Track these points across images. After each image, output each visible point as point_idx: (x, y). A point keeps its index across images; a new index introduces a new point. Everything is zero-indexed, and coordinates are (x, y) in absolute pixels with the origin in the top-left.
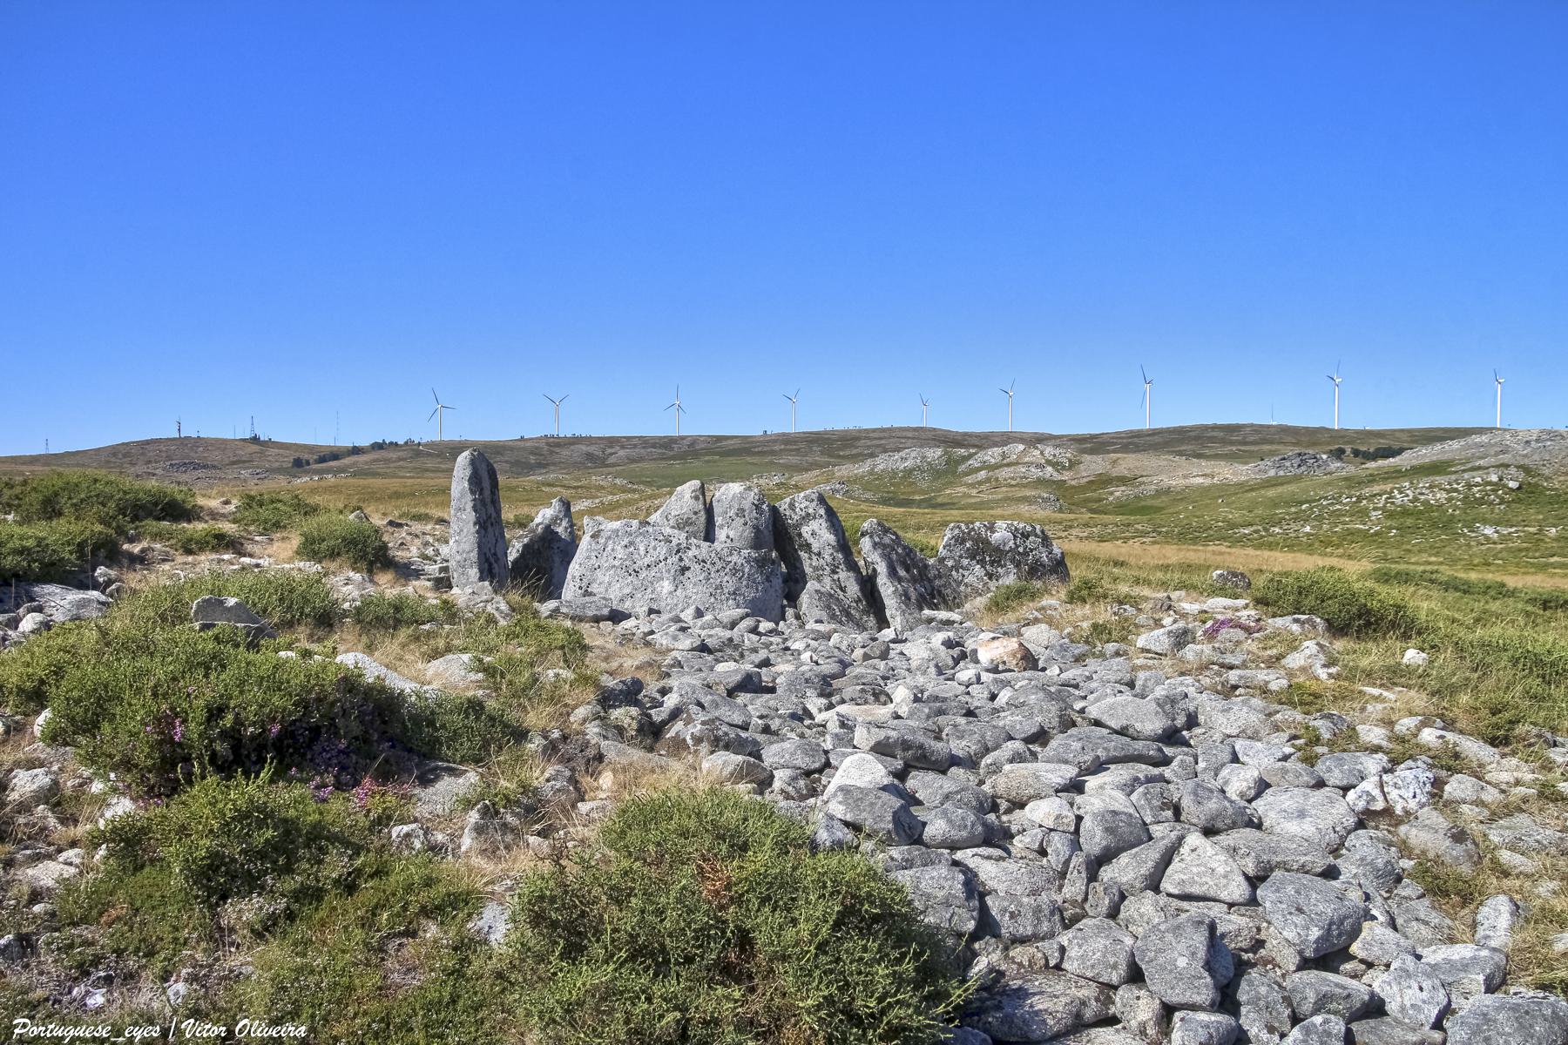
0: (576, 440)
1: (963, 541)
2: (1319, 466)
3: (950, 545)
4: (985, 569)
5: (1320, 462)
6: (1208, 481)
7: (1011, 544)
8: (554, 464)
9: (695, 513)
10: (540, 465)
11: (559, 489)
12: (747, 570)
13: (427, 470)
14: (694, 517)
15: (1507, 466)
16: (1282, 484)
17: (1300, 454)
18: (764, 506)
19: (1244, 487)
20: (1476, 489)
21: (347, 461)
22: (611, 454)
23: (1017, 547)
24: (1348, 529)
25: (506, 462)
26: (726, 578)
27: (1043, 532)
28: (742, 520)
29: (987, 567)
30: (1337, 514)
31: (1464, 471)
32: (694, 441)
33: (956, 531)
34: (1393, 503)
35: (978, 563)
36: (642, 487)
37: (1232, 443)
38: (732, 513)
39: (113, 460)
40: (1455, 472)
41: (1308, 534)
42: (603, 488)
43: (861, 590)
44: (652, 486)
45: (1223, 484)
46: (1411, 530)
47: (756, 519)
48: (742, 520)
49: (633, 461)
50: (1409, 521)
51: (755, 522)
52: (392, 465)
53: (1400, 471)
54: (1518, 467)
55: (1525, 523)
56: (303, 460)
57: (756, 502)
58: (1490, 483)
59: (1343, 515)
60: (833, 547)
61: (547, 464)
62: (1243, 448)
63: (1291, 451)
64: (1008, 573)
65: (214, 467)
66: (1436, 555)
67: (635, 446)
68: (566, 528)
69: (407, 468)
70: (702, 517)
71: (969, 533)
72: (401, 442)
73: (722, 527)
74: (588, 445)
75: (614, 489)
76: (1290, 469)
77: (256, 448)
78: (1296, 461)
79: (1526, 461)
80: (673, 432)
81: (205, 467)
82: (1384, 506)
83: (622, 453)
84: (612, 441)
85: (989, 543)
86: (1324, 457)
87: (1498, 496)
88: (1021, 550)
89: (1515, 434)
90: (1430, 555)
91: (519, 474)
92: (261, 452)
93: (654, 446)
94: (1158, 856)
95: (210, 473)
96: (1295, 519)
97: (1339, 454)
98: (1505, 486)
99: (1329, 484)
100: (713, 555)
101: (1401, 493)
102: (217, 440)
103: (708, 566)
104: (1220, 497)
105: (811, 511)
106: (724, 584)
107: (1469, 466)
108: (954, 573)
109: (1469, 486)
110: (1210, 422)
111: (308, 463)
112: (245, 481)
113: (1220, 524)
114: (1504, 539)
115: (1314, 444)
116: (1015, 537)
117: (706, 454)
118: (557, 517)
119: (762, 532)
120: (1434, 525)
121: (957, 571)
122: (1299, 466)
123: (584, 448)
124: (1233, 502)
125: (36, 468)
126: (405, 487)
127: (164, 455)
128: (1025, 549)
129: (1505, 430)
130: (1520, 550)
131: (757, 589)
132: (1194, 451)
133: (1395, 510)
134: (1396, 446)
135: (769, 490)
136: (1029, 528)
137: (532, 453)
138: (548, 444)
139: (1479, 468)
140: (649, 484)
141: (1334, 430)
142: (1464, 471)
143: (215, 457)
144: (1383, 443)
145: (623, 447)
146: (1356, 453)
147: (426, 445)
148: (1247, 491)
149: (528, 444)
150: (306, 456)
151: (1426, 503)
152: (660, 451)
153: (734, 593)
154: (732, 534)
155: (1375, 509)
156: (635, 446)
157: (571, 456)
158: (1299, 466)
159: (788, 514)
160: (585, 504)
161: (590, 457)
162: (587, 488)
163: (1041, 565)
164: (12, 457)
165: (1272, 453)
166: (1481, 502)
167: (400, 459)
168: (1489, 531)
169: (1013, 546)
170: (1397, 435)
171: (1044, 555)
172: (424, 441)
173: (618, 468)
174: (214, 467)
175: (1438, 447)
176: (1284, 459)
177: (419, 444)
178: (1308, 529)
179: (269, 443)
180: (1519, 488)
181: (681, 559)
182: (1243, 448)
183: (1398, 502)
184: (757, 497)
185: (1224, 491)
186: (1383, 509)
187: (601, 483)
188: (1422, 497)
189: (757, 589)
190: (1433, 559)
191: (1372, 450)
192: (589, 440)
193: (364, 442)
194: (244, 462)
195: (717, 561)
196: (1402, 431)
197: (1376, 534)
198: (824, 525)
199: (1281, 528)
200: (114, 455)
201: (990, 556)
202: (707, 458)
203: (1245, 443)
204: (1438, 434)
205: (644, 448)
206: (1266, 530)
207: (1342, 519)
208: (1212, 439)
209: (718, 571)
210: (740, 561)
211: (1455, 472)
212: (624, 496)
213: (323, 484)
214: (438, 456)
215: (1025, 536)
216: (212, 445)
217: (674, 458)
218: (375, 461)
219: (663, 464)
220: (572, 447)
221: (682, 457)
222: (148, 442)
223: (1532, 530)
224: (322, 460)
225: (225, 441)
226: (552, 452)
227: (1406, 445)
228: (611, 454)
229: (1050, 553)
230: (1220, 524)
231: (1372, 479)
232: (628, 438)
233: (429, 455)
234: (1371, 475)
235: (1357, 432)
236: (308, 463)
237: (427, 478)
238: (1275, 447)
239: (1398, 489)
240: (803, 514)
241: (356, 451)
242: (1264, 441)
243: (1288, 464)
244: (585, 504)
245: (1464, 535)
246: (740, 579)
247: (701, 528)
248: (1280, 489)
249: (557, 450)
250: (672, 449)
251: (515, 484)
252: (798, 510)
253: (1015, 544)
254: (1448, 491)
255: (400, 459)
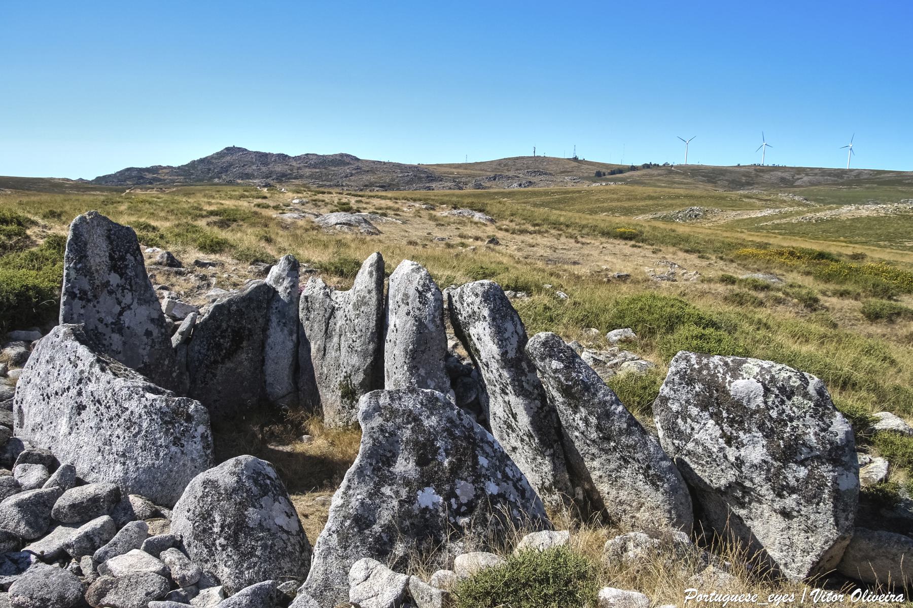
0: (775, 168)
1: (690, 382)
3: (673, 382)
4: (722, 429)
7: (760, 400)
8: (758, 183)
10: (748, 184)
11: (754, 200)
12: (145, 425)
13: (675, 183)
18: (429, 295)
21: (627, 174)
22: (798, 179)
23: (768, 408)
25: (726, 180)
26: (119, 431)
27: (820, 392)
29: (725, 426)
32: (860, 173)
33: (683, 365)
35: (711, 415)
36: (813, 203)
39: (499, 167)
42: (785, 202)
43: (532, 423)
44: (820, 203)
47: (419, 309)
49: (812, 184)
51: (417, 312)
52: (654, 178)
56: (602, 173)
57: (420, 289)
60: (498, 361)
61: (753, 183)
64: (755, 444)
65: (550, 174)
67: (816, 174)
68: (287, 288)
69: (663, 180)
70: (374, 301)
71: (700, 371)
72: (661, 164)
74: (782, 172)
75: (793, 203)
77: (576, 164)
80: (846, 167)
81: (546, 174)
83: (806, 179)
84: (800, 170)
85: (726, 392)
88: (774, 414)
91: (734, 189)
92: (579, 167)
93: (829, 175)
95: (547, 177)
100: (109, 395)
102: (554, 158)
103: (102, 409)
106: (114, 439)
108: (679, 421)
111: (604, 175)
112: (567, 183)
116: (767, 391)
117: (867, 183)
119: (426, 327)
121: (684, 420)
123: (779, 174)
125: (460, 171)
126: (656, 192)
127: (525, 166)
128: (780, 414)
131: (157, 454)
135: (905, 212)
136: (795, 382)
137: (744, 175)
138: (756, 170)
140: (816, 200)
143: (552, 168)
145: (807, 175)
147: (677, 167)
149: (742, 169)
150: (604, 170)
152: (833, 179)
153: (124, 455)
156: (816, 174)
157: (770, 179)
160: (769, 212)
161: (783, 180)
162: (774, 201)
163: (804, 444)
164: (450, 164)
167: (659, 175)
169: (762, 406)
171: (811, 431)
172: (675, 164)
173: (802, 189)
174: (550, 174)
177: (672, 166)
179: (583, 162)
181: (80, 393)
184: (422, 282)
187: (785, 198)
189: (157, 454)
192: (784, 169)
193: (639, 163)
194: (569, 172)
195: (112, 403)
198: (488, 330)
200: (500, 165)
201: (728, 411)
202: (867, 186)
205: (822, 176)
209: (111, 419)
210: (137, 411)
212: (796, 208)
213: (607, 188)
214: (683, 174)
215: (787, 393)
216: (551, 161)
217: (843, 184)
218: (644, 175)
219: (834, 188)
220: (772, 173)
221: (849, 183)
222: (517, 158)
224: (613, 173)
225: (559, 159)
226: (757, 176)
228: (798, 179)
229: (823, 430)
232: (812, 169)
233: (677, 173)
236: (604, 175)
237: (674, 188)
241: (633, 168)
244: (769, 212)
246: (135, 436)
249: (761, 174)
250: (842, 178)
251: (725, 195)
253: (765, 403)
255: (659, 175)
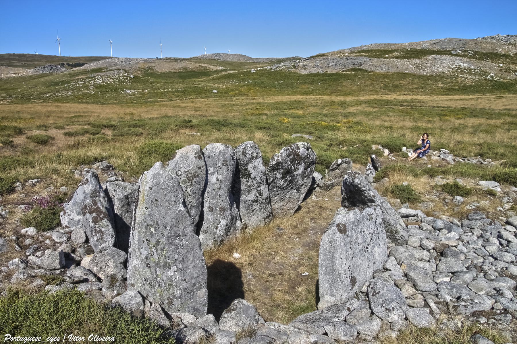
2: (58, 70)
5: (58, 68)
6: (17, 76)
9: (200, 168)
14: (199, 171)
15: (120, 70)
16: (46, 76)
17: (50, 65)
19: (32, 78)
20: (121, 78)
24: (84, 93)
28: (226, 168)
30: (78, 88)
31: (107, 71)
34: (96, 83)
37: (22, 61)
38: (219, 164)
40: (104, 72)
41: (70, 95)
45: (23, 77)
46: (105, 92)
48: (226, 168)
50: (104, 89)
53: (87, 71)
54: (123, 70)
55: (138, 89)
58: (125, 76)
59: (81, 88)
62: (27, 63)
63: (47, 64)
66: (116, 100)
73: (213, 174)
76: (47, 71)
78: (49, 68)
79: (125, 68)
82: (94, 84)
86: (59, 66)
87: (128, 80)
89: (118, 59)
90: (114, 101)
94: (206, 289)
96: (64, 90)
97: (63, 65)
98: (130, 77)
99: (63, 76)
101: (98, 80)
104: (23, 81)
105: (255, 155)
107: (108, 69)
109: (119, 77)
110: (12, 53)
113: (36, 93)
114: (134, 94)
115: (53, 62)
118: (96, 190)
120: (112, 90)
122: (51, 70)
124: (29, 84)
129: (115, 58)
130: (140, 97)
132: (7, 64)
133: (98, 86)
134: (82, 63)
139: (111, 70)
141: (59, 57)
142: (107, 71)
144: (77, 61)
146: (69, 65)
148: (33, 79)
151: (107, 83)
154: (220, 177)
155: (91, 86)
158: (51, 70)
159: (241, 158)
165: (39, 65)
166: (123, 82)
168: (128, 91)
170: (81, 59)
175: (96, 63)
176: (45, 67)
178: (70, 93)
180: (134, 78)
182: (27, 63)
183: (98, 83)
185: (24, 79)
186: (93, 85)
188: (105, 81)
190: (115, 102)
191: (74, 64)
196: (82, 57)
197: (94, 94)
199: (60, 93)
203: (27, 61)
204: (94, 58)
206: (54, 94)
207: (81, 89)
208: (14, 59)
211: (104, 72)
223: (140, 90)
227: (84, 62)
230: (36, 93)
231: (78, 74)
234: (77, 73)
235: (67, 57)
238: (39, 63)
239: (97, 78)
240: (250, 157)
242: (34, 60)
243: (46, 69)
245: (122, 93)
247: (204, 178)
248: (46, 78)
252: (248, 155)
254: (113, 79)
